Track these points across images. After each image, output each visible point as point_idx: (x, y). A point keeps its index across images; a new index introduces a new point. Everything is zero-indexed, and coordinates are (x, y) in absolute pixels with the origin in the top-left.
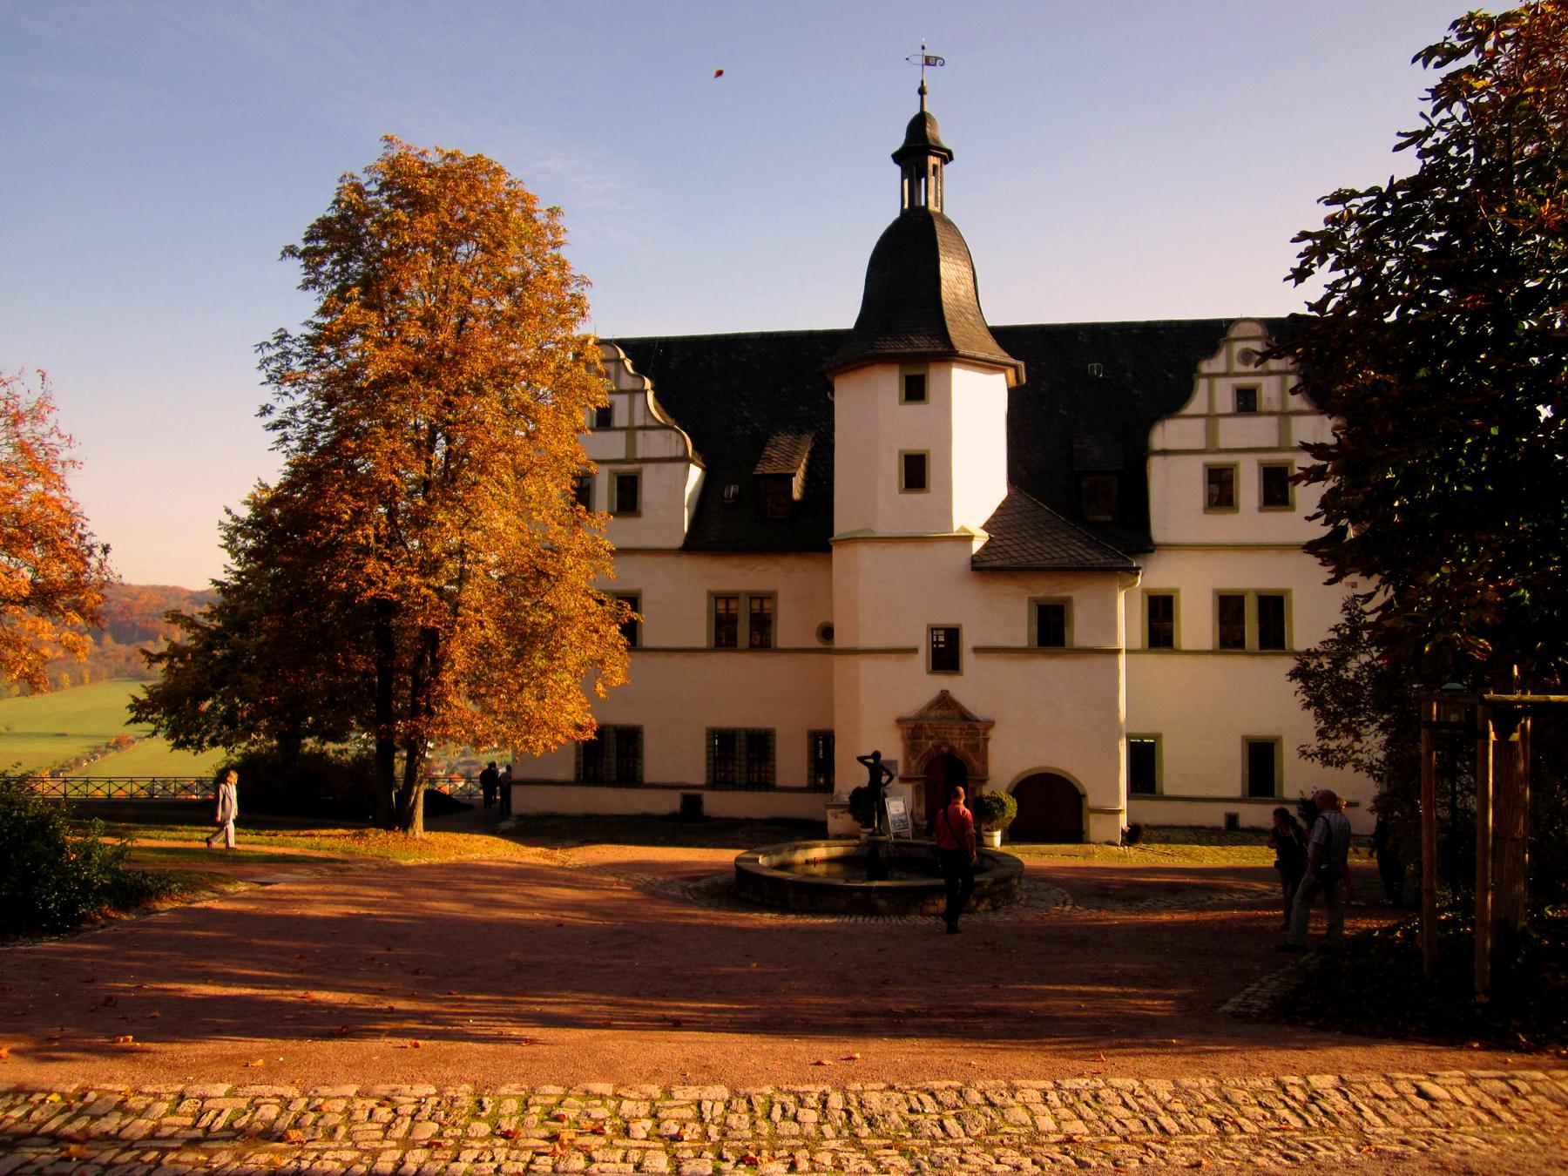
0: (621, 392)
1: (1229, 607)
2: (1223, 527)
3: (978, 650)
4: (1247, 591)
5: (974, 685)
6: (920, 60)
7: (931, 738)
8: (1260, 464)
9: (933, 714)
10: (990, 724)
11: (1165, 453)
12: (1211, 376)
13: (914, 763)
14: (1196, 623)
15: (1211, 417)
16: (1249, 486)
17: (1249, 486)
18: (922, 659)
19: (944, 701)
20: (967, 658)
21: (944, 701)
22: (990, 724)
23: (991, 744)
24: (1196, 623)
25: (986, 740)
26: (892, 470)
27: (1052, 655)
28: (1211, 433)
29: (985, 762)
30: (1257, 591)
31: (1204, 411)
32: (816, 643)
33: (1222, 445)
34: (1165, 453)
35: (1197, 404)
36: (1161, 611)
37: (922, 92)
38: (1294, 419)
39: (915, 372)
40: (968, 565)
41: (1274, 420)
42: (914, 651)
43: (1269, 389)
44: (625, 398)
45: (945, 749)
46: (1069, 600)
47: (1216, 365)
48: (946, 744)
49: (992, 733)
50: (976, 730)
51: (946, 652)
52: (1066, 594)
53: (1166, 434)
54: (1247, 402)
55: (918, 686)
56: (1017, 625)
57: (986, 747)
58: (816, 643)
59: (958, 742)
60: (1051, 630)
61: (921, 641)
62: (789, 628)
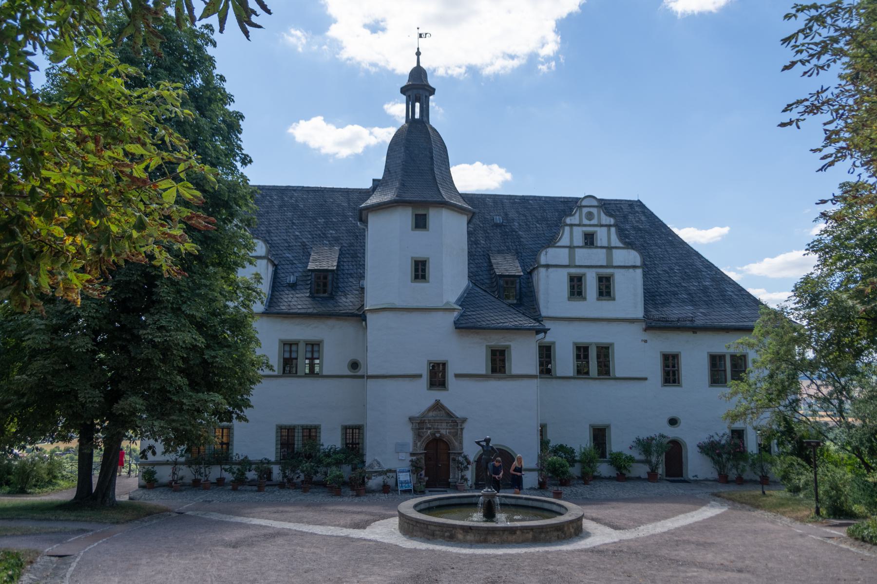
0: (602, 226)
1: (582, 352)
2: (577, 309)
3: (457, 376)
4: (591, 344)
5: (457, 397)
6: (417, 36)
7: (430, 429)
8: (569, 274)
9: (431, 414)
10: (464, 420)
11: (547, 266)
12: (571, 225)
13: (419, 444)
14: (564, 362)
15: (571, 248)
16: (591, 286)
17: (591, 286)
18: (424, 381)
19: (437, 406)
20: (451, 380)
21: (437, 406)
22: (464, 420)
23: (465, 431)
24: (564, 362)
25: (462, 429)
26: (408, 269)
27: (500, 379)
28: (572, 257)
29: (461, 443)
30: (596, 344)
31: (568, 244)
32: (347, 372)
33: (577, 264)
34: (547, 266)
35: (565, 240)
36: (546, 353)
37: (418, 54)
38: (614, 251)
39: (421, 212)
40: (452, 326)
41: (604, 250)
42: (420, 376)
43: (602, 236)
44: (605, 229)
45: (438, 435)
46: (508, 347)
47: (574, 220)
48: (439, 432)
49: (465, 425)
50: (456, 423)
51: (437, 376)
52: (507, 343)
53: (548, 256)
54: (589, 240)
55: (419, 398)
56: (480, 363)
57: (462, 434)
58: (347, 372)
59: (444, 431)
60: (498, 362)
61: (425, 372)
62: (333, 360)
